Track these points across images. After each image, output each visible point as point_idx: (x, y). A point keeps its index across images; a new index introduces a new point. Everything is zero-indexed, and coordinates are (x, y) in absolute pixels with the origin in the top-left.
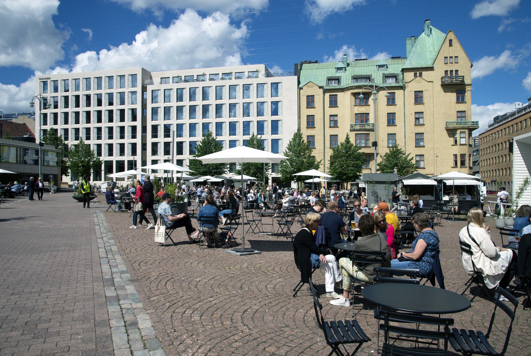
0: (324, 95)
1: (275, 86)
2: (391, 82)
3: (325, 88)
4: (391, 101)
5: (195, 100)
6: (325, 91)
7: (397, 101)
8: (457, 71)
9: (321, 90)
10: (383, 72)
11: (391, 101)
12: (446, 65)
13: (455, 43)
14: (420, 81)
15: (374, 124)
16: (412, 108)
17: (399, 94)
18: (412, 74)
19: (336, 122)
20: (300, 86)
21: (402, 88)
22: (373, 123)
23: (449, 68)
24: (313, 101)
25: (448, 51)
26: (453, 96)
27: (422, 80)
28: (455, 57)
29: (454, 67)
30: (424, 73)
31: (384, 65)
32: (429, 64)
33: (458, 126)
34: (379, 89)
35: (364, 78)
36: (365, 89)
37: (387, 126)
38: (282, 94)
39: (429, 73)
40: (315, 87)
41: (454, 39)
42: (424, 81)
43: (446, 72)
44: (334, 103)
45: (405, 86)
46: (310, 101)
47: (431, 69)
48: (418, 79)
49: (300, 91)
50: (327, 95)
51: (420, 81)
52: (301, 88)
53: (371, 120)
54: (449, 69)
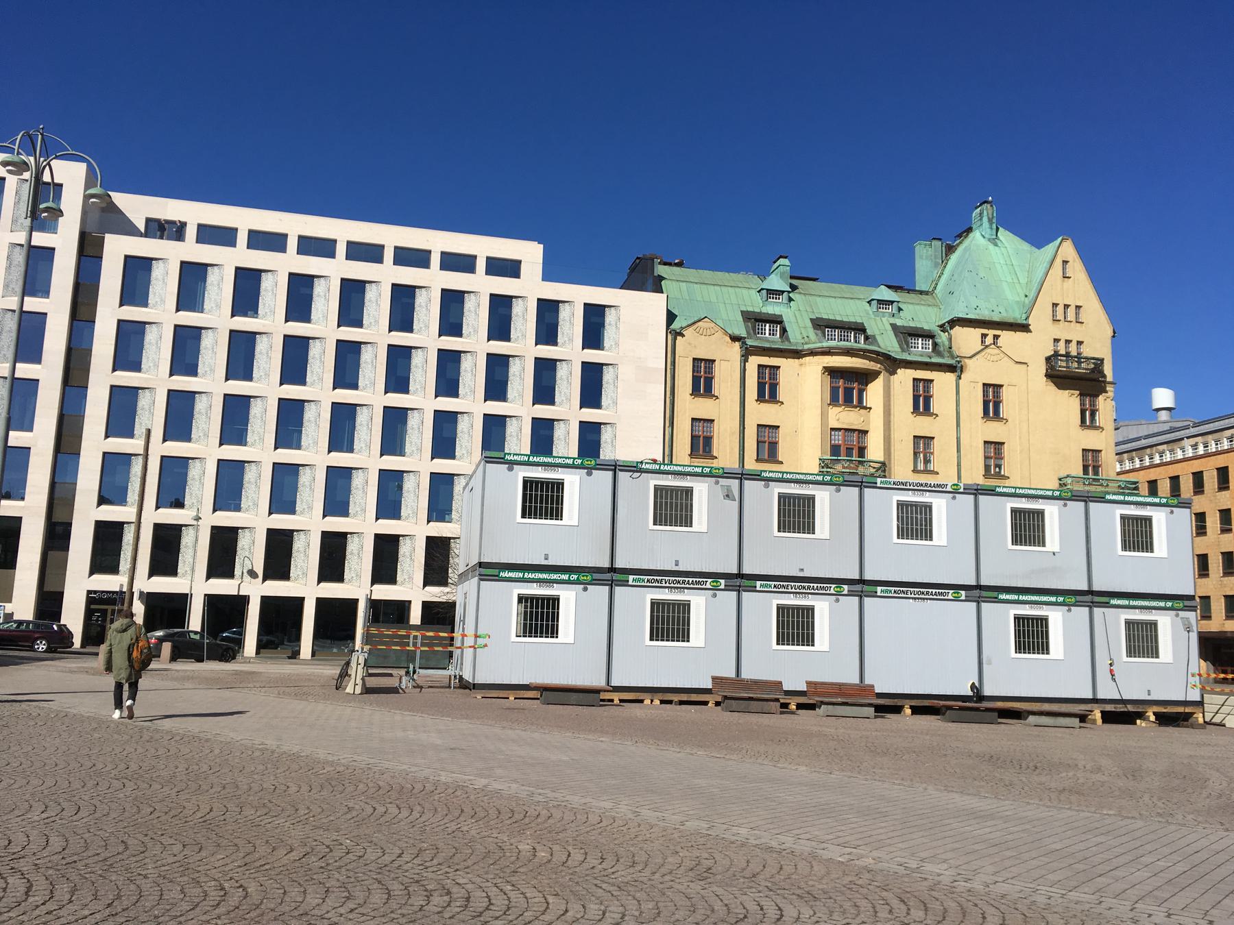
0: (746, 361)
1: (595, 319)
2: (921, 349)
3: (750, 342)
4: (922, 403)
5: (144, 303)
6: (747, 352)
7: (935, 406)
8: (1080, 343)
9: (737, 344)
10: (893, 321)
11: (922, 403)
12: (1057, 325)
13: (1077, 269)
14: (995, 358)
15: (883, 464)
16: (978, 431)
17: (943, 382)
18: (975, 334)
19: (773, 446)
20: (676, 325)
21: (955, 368)
22: (882, 459)
23: (1063, 331)
24: (299, 422)
25: (1055, 290)
26: (1069, 402)
27: (1002, 355)
28: (1077, 307)
29: (1072, 332)
30: (1006, 337)
31: (892, 302)
32: (1016, 316)
33: (1092, 488)
34: (892, 364)
35: (854, 329)
36: (870, 359)
37: (757, 401)
38: (617, 344)
39: (1020, 336)
40: (720, 334)
41: (1074, 261)
42: (1006, 358)
43: (1056, 341)
44: (768, 390)
45: (962, 367)
46: (703, 383)
47: (1024, 328)
48: (992, 350)
49: (675, 339)
50: (754, 361)
51: (995, 358)
52: (679, 334)
53: (875, 452)
54: (1064, 336)
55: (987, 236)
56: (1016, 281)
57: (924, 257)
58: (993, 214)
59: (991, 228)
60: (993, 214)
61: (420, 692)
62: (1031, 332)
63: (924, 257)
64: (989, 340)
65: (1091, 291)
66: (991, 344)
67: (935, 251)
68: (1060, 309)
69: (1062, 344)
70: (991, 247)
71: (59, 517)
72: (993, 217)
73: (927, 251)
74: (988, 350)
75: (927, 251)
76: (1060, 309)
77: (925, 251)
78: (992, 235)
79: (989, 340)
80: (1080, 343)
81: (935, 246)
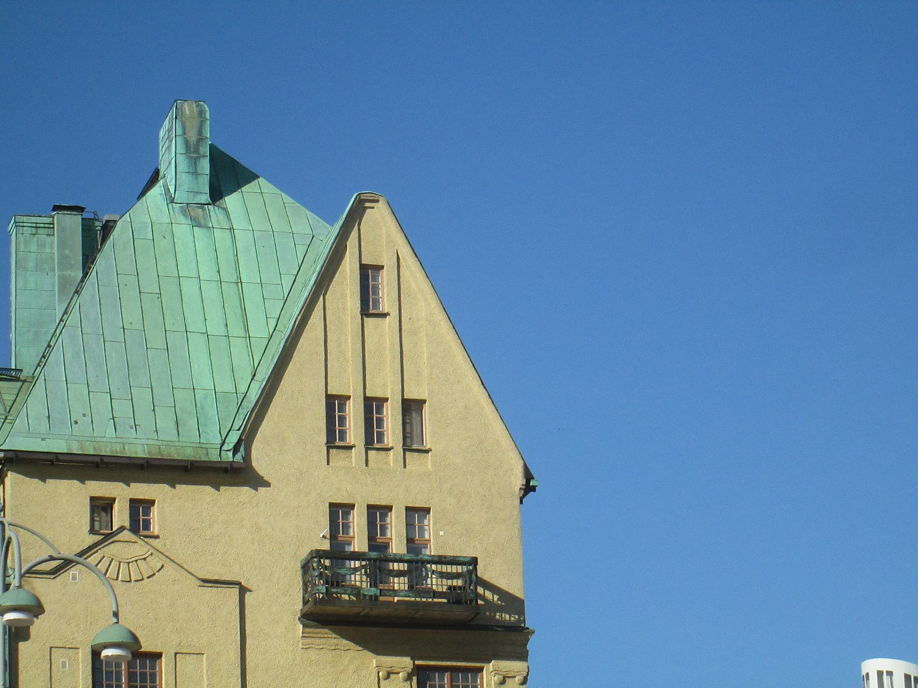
8: (416, 514)
55: (180, 196)
56: (236, 330)
57: (31, 265)
58: (200, 132)
59: (195, 174)
60: (200, 132)
61: (139, 425)
62: (267, 484)
63: (31, 265)
64: (120, 516)
65: (89, 512)
66: (122, 529)
67: (62, 245)
68: (354, 413)
69: (358, 522)
70: (183, 229)
71: (410, 536)
72: (201, 139)
73: (42, 245)
74: (111, 550)
75: (42, 245)
76: (354, 413)
77: (33, 247)
78: (197, 193)
79: (120, 516)
80: (416, 514)
81: (62, 230)
